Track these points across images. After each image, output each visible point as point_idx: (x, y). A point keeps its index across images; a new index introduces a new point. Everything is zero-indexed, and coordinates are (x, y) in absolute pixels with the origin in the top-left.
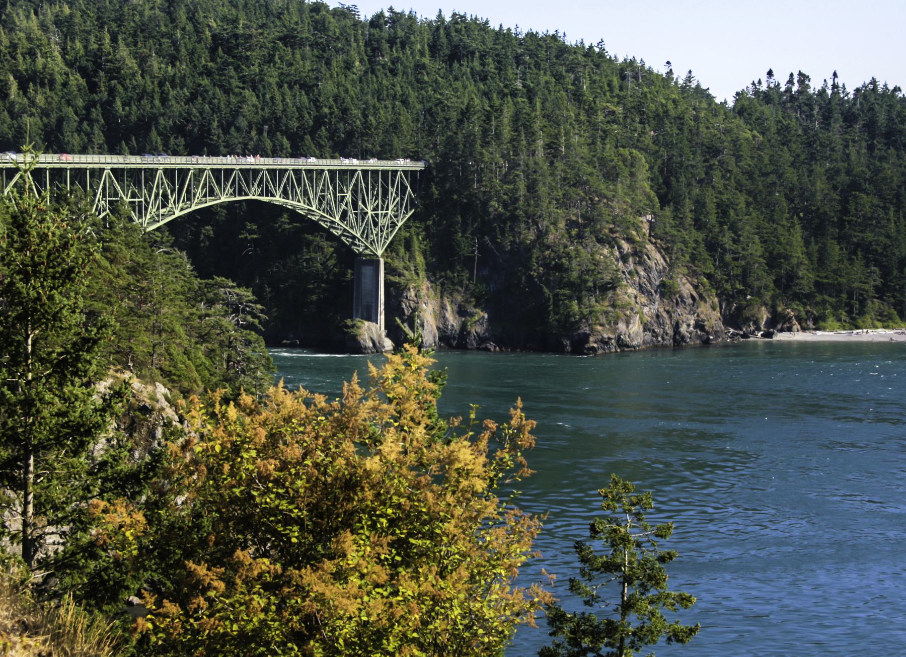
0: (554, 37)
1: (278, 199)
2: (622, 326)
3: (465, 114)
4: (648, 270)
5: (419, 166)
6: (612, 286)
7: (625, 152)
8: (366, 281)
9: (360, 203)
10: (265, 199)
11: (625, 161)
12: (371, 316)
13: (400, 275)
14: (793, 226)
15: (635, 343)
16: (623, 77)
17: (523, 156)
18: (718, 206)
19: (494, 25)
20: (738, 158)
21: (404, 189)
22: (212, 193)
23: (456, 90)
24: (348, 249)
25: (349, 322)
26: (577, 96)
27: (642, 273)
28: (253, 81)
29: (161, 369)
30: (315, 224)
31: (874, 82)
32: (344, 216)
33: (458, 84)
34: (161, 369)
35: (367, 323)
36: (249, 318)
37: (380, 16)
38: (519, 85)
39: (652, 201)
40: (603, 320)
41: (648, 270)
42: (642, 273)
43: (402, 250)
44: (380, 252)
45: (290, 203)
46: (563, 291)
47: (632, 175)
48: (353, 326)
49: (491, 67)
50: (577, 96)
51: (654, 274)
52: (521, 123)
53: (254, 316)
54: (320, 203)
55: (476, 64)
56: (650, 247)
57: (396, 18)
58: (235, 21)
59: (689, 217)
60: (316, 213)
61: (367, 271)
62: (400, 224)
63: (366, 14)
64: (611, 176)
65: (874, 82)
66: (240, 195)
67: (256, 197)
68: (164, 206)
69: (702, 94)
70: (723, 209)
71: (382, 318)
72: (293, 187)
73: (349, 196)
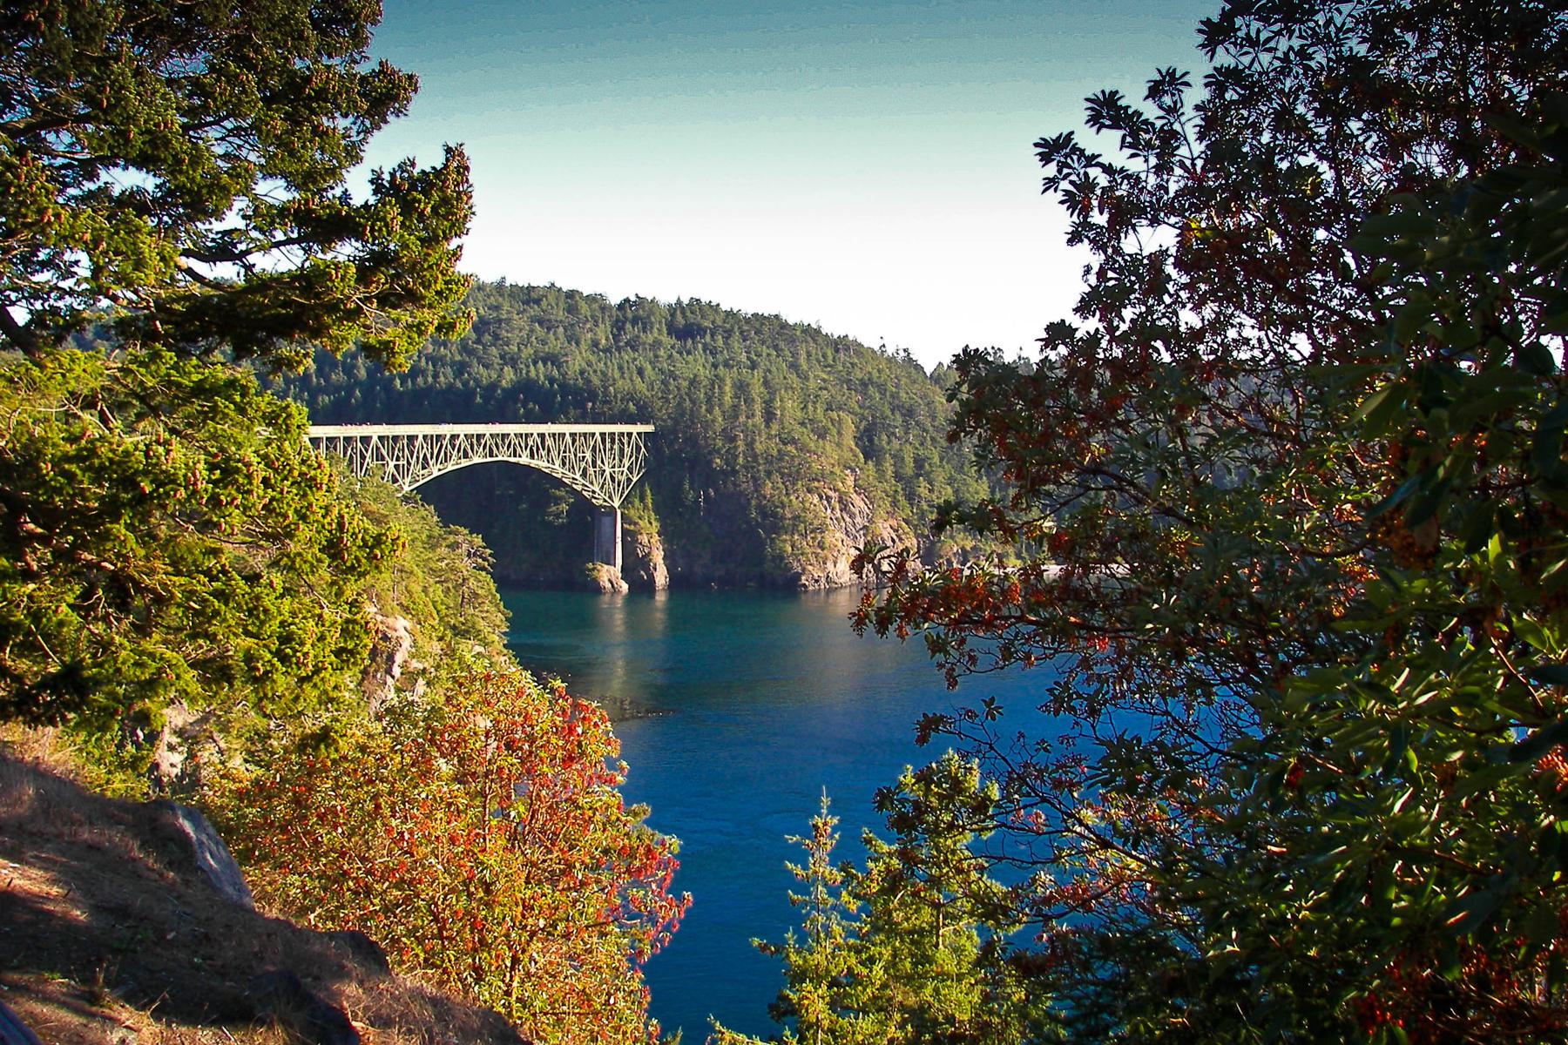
0: (777, 316)
1: (524, 460)
2: (830, 565)
3: (694, 382)
4: (852, 516)
5: (650, 428)
6: (822, 529)
7: (834, 415)
8: (606, 529)
9: (599, 462)
10: (512, 460)
11: (832, 420)
12: (610, 561)
13: (636, 524)
14: (981, 478)
15: (842, 581)
16: (837, 351)
17: (742, 419)
18: (915, 461)
19: (725, 307)
20: (934, 418)
21: (638, 449)
22: (466, 456)
23: (687, 363)
24: (587, 502)
25: (590, 566)
26: (794, 366)
27: (848, 519)
28: (512, 359)
29: (401, 604)
30: (560, 481)
31: (1063, 321)
32: (584, 475)
33: (690, 358)
34: (401, 604)
35: (606, 567)
36: (480, 561)
37: (627, 300)
38: (744, 357)
39: (855, 456)
40: (813, 560)
41: (852, 516)
42: (848, 519)
43: (637, 502)
44: (616, 504)
45: (534, 463)
46: (289, 450)
47: (839, 433)
48: (594, 569)
49: (720, 342)
50: (794, 366)
51: (858, 520)
52: (741, 388)
53: (484, 559)
54: (564, 464)
55: (708, 338)
56: (854, 496)
57: (641, 301)
58: (497, 308)
59: (890, 473)
60: (558, 471)
61: (607, 520)
62: (635, 480)
63: (615, 299)
64: (822, 434)
65: (1063, 321)
66: (491, 456)
67: (505, 458)
68: (424, 468)
69: (910, 363)
70: (919, 463)
71: (619, 561)
72: (538, 449)
73: (588, 455)
